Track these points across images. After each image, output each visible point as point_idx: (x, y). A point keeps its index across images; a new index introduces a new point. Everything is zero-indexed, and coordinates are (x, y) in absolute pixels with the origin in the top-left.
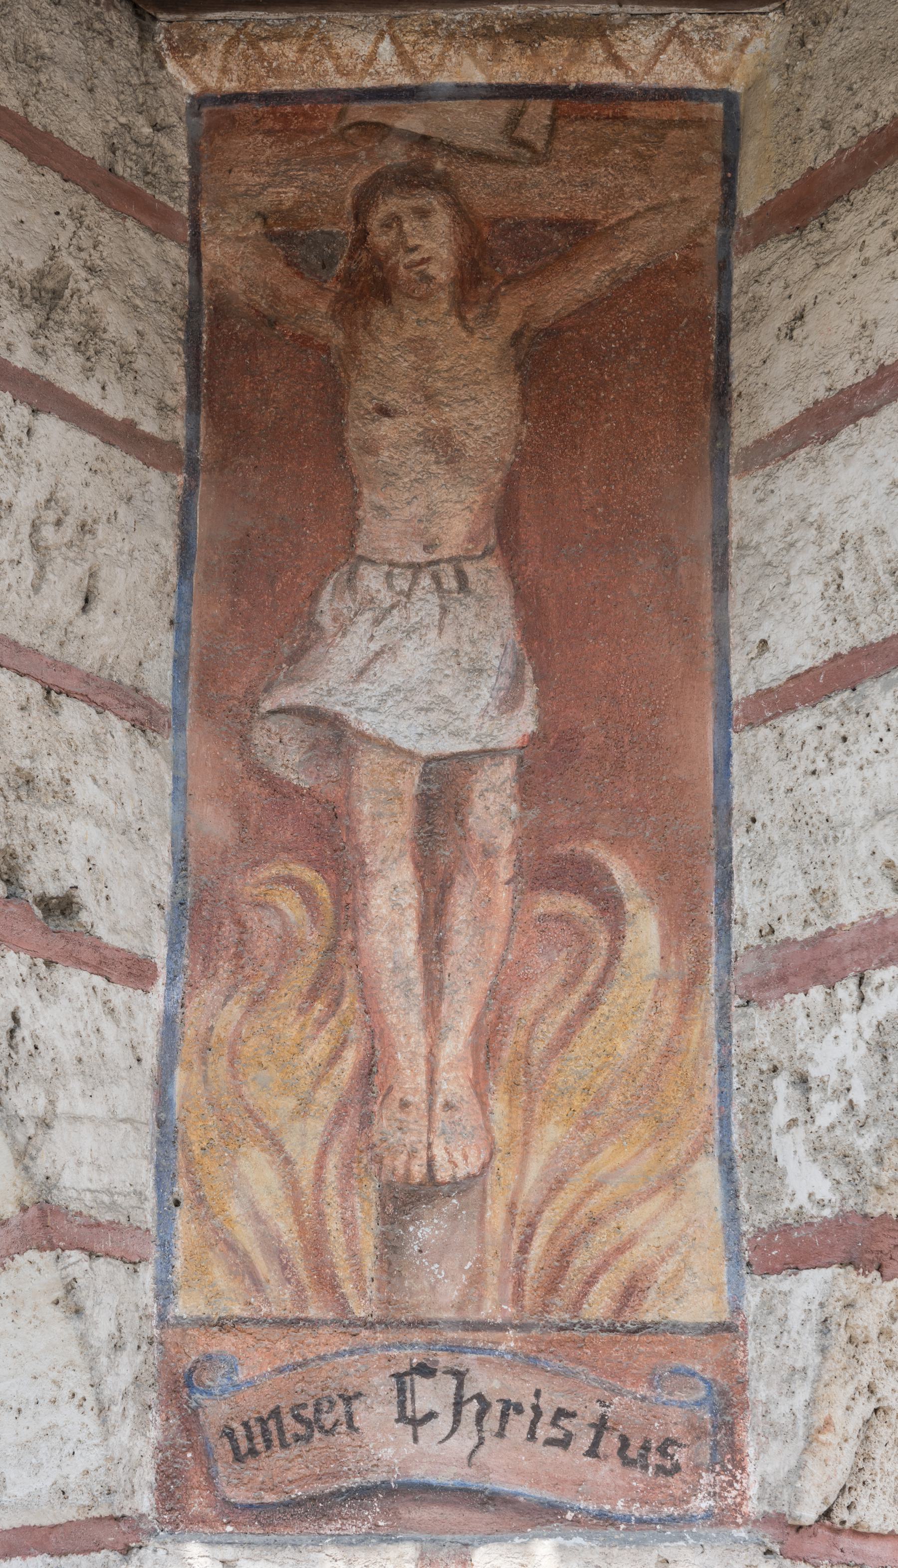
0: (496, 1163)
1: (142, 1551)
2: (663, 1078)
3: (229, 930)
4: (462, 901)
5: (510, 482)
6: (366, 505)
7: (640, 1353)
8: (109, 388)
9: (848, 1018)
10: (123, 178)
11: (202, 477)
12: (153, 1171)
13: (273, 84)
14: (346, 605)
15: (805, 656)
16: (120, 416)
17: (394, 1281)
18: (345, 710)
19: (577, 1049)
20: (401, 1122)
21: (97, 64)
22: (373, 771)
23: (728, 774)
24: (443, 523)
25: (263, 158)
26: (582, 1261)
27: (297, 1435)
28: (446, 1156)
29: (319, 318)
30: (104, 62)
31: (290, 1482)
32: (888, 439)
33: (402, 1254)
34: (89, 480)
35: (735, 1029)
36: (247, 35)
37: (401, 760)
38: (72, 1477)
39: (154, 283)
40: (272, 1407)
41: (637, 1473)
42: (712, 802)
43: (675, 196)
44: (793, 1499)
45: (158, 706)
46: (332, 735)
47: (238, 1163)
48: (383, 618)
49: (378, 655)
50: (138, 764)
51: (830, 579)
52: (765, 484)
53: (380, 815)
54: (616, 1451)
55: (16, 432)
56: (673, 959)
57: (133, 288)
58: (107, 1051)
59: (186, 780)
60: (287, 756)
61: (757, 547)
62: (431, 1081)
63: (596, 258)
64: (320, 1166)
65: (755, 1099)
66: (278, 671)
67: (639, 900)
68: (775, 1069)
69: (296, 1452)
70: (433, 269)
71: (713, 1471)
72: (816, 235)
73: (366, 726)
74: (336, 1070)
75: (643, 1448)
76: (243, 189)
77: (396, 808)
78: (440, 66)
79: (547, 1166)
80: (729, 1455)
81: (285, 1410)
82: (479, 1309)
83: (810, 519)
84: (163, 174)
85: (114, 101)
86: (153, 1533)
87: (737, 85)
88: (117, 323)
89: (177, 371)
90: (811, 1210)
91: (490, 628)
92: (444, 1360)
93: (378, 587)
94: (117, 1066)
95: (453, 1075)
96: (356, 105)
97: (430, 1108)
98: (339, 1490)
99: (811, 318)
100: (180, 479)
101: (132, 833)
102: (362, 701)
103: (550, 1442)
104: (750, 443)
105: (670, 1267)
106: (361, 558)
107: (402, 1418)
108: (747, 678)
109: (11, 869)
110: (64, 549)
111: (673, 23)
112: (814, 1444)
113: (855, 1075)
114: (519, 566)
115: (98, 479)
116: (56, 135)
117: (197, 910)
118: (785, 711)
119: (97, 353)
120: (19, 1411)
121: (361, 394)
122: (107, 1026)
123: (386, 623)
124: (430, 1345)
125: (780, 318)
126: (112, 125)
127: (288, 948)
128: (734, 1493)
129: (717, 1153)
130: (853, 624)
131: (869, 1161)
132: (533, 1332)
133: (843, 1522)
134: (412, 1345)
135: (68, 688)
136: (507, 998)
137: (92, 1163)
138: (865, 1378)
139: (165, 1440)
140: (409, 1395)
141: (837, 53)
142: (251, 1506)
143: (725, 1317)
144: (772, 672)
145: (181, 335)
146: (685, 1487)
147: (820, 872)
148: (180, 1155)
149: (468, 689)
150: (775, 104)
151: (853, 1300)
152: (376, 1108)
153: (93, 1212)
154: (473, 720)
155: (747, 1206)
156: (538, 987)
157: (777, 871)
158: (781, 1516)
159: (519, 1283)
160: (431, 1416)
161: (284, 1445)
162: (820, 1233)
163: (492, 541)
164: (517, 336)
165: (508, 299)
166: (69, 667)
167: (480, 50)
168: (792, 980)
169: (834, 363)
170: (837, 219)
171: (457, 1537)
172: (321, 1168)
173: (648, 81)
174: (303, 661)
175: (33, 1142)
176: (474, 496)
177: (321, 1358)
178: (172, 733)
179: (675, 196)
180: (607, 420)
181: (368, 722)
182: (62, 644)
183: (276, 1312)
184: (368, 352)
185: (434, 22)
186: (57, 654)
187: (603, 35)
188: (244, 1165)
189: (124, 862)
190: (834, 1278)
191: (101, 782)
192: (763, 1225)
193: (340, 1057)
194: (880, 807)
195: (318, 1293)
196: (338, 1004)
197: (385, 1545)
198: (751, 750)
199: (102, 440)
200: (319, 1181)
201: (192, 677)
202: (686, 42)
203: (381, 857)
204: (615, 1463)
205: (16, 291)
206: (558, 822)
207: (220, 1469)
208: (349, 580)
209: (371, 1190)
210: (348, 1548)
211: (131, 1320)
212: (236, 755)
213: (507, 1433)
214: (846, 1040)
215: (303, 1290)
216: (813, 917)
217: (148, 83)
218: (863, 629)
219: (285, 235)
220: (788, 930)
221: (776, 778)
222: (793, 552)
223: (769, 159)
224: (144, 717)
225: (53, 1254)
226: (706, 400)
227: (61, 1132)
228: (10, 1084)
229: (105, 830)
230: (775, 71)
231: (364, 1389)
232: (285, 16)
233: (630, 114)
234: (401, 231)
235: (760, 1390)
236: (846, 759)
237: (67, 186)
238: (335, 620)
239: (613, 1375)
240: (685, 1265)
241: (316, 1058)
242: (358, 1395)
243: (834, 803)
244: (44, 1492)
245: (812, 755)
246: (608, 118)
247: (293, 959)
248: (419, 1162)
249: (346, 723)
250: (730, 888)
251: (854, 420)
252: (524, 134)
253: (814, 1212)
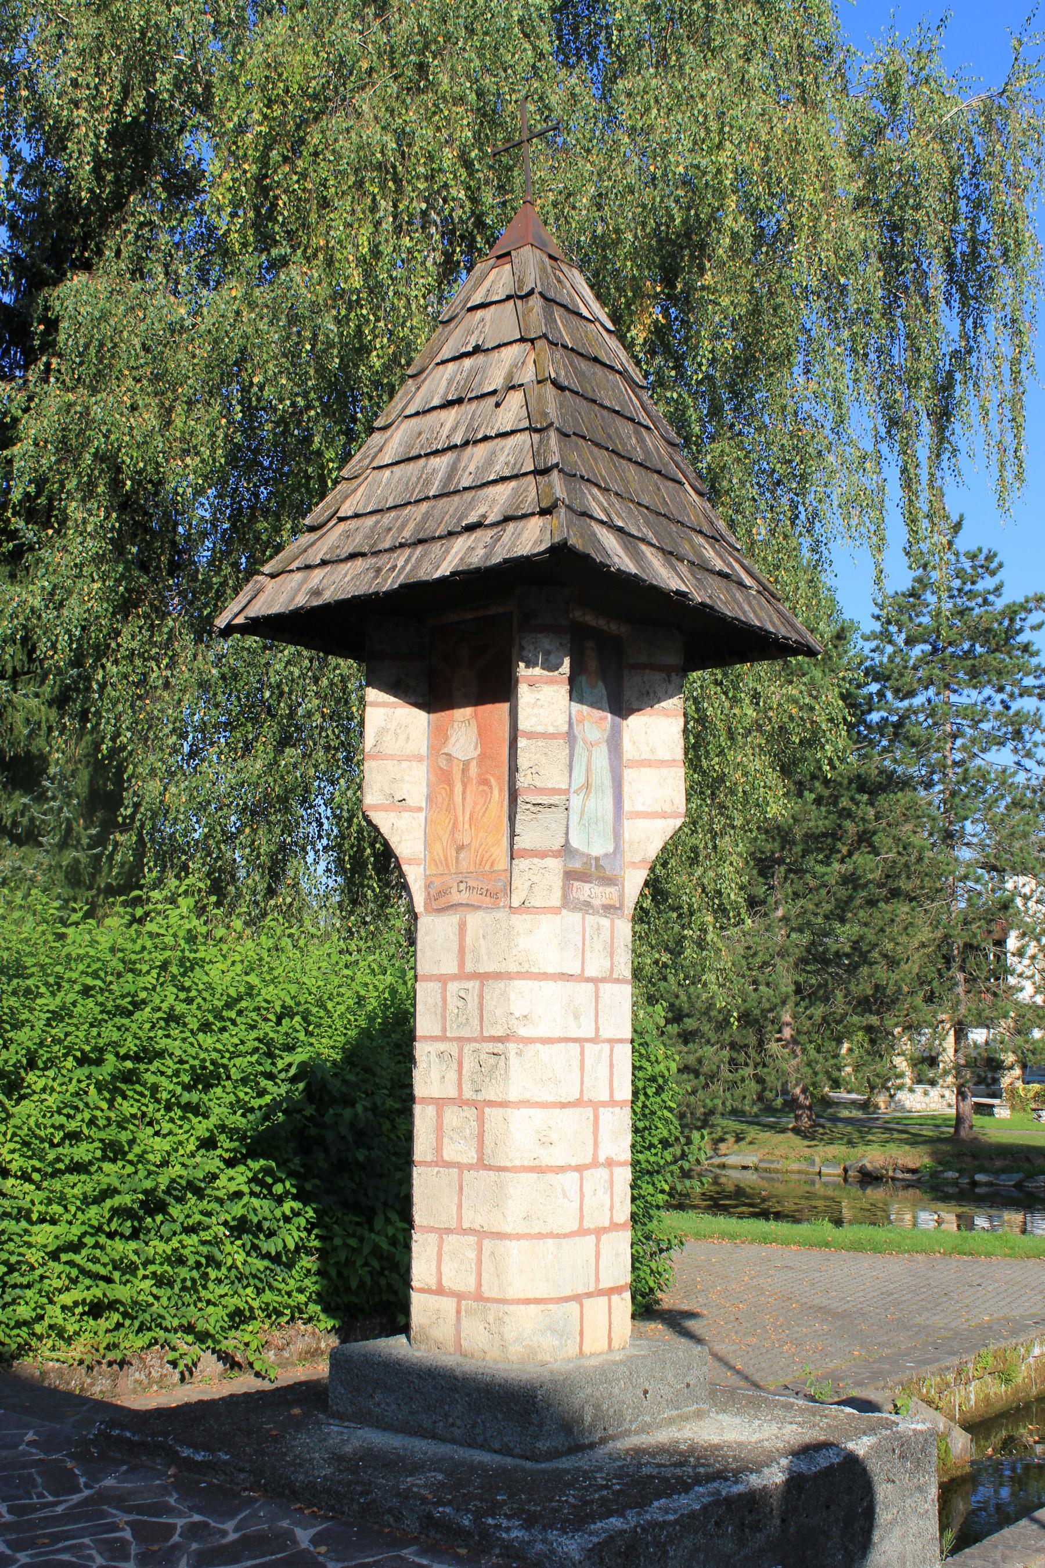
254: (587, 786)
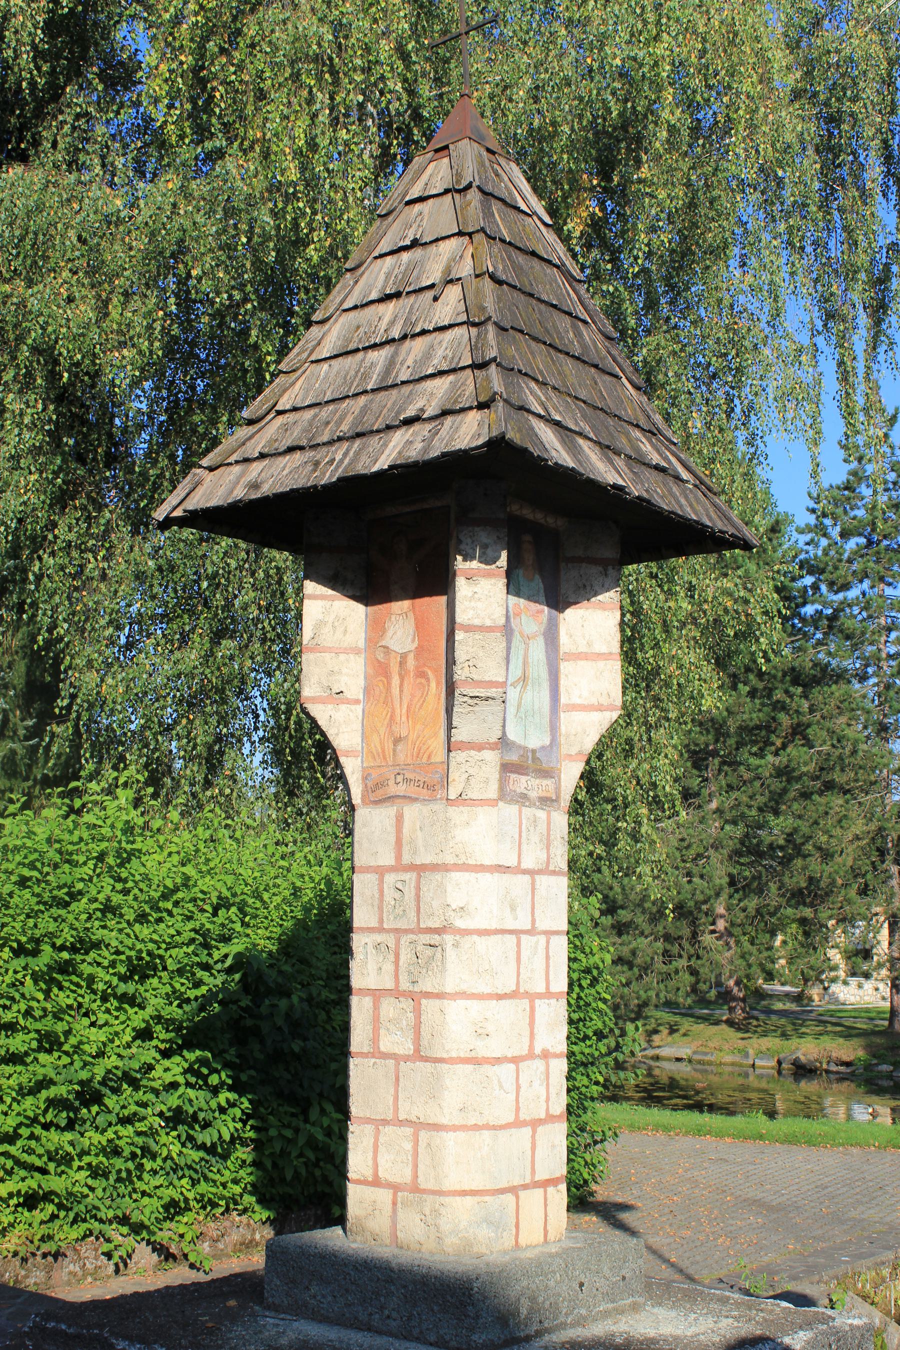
254: (524, 679)
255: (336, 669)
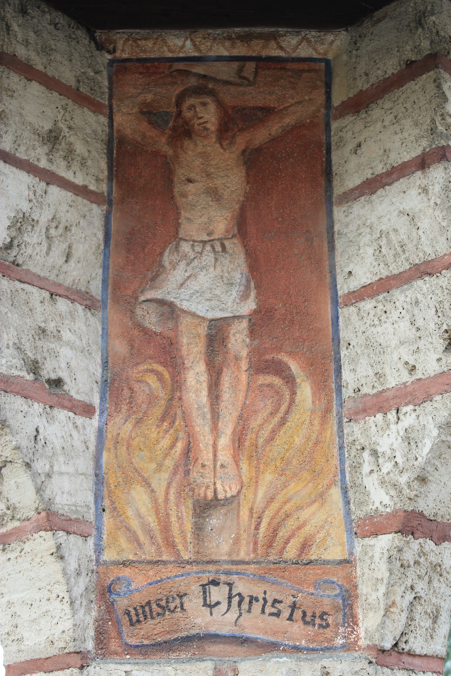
0: (244, 490)
1: (89, 668)
2: (315, 453)
3: (126, 393)
4: (226, 379)
5: (243, 209)
6: (182, 218)
7: (310, 574)
8: (77, 174)
9: (393, 427)
10: (82, 92)
11: (114, 206)
12: (93, 496)
13: (143, 55)
14: (175, 257)
15: (367, 278)
16: (81, 184)
17: (200, 543)
18: (175, 300)
19: (278, 441)
20: (202, 473)
21: (73, 51)
22: (187, 325)
23: (338, 325)
24: (215, 225)
25: (138, 83)
26: (283, 533)
27: (158, 613)
28: (222, 488)
29: (163, 144)
30: (76, 50)
31: (156, 634)
32: (397, 195)
33: (204, 531)
34: (69, 209)
35: (345, 432)
36: (132, 38)
37: (200, 320)
38: (57, 634)
39: (95, 132)
40: (147, 600)
41: (310, 628)
42: (331, 337)
43: (307, 98)
44: (380, 638)
45: (96, 299)
46: (170, 310)
47: (131, 492)
48: (191, 263)
49: (189, 277)
50: (88, 323)
51: (376, 248)
52: (348, 210)
53: (191, 344)
54: (300, 618)
55: (40, 193)
56: (317, 403)
57: (86, 134)
58: (74, 444)
59: (107, 329)
60: (151, 319)
61: (346, 234)
62: (215, 455)
63: (275, 121)
64: (167, 493)
65: (355, 461)
66: (147, 284)
67: (302, 378)
68: (363, 449)
69: (158, 621)
70: (209, 126)
71: (344, 626)
72: (364, 116)
73: (184, 307)
74: (173, 452)
75: (312, 616)
76: (130, 95)
77: (197, 340)
78: (210, 50)
79: (266, 492)
80: (351, 619)
81: (153, 602)
82: (238, 555)
83: (367, 224)
84: (98, 90)
85: (79, 64)
86: (93, 659)
87: (330, 56)
88: (80, 148)
89: (104, 165)
90: (381, 509)
91: (236, 266)
92: (223, 578)
93: (188, 250)
94: (79, 451)
95: (224, 453)
96: (176, 63)
97: (215, 467)
98: (177, 638)
99: (364, 147)
100: (105, 207)
101: (85, 352)
102: (182, 297)
103: (271, 614)
104: (341, 193)
105: (321, 535)
106: (181, 239)
107: (205, 605)
108: (343, 288)
109: (36, 368)
110: (58, 238)
111: (304, 35)
112: (388, 613)
113: (397, 451)
114: (247, 242)
115: (72, 209)
116: (57, 78)
117: (113, 383)
118: (360, 300)
119: (72, 160)
120: (32, 605)
121: (180, 174)
122: (75, 434)
123: (192, 265)
124: (217, 572)
125: (351, 146)
126: (79, 73)
127: (152, 399)
128: (354, 636)
129: (340, 485)
130: (387, 266)
131: (405, 487)
132: (262, 565)
133: (403, 649)
134: (209, 572)
135: (60, 293)
136: (247, 420)
137: (68, 493)
138: (409, 583)
139: (99, 616)
140: (208, 594)
141: (369, 48)
142: (138, 646)
143: (346, 557)
144: (354, 284)
145: (105, 151)
146: (332, 634)
147: (378, 366)
148: (105, 489)
149: (227, 292)
150: (346, 65)
151: (402, 548)
152: (191, 467)
153: (68, 514)
154: (229, 304)
155: (354, 508)
156: (260, 415)
157: (360, 366)
158: (375, 646)
159: (256, 543)
160: (218, 603)
161: (152, 618)
162: (386, 519)
163: (236, 232)
164: (244, 152)
165: (240, 137)
166: (60, 285)
167: (226, 44)
168: (368, 411)
169: (373, 164)
170: (372, 110)
171: (231, 658)
172: (167, 494)
173: (294, 55)
174: (157, 280)
175: (44, 484)
176: (228, 214)
177: (169, 578)
178: (101, 310)
179: (307, 98)
180: (282, 184)
181: (185, 305)
182: (57, 275)
183: (148, 558)
184: (182, 157)
185: (208, 34)
186: (55, 280)
187: (275, 39)
188: (133, 493)
189: (82, 364)
190: (393, 538)
191: (73, 331)
192: (361, 516)
193: (175, 445)
194: (402, 340)
195: (167, 549)
196: (174, 423)
197: (199, 663)
198: (347, 316)
199: (74, 194)
200: (167, 499)
201: (110, 287)
202: (309, 41)
203: (191, 361)
204: (301, 623)
205: (41, 138)
206: (267, 346)
207: (124, 629)
208: (176, 248)
209: (190, 504)
210: (182, 664)
211: (84, 561)
212: (129, 319)
213: (252, 611)
214: (393, 436)
215: (160, 548)
216: (376, 384)
217: (92, 56)
218: (391, 268)
219: (149, 113)
220: (365, 390)
221: (358, 327)
222: (361, 237)
223: (344, 85)
224: (90, 304)
225: (52, 533)
226: (322, 176)
227: (55, 479)
228: (35, 459)
229: (74, 351)
230: (345, 53)
231: (188, 592)
232: (148, 31)
233: (287, 67)
234: (195, 111)
235: (364, 589)
236: (386, 320)
237: (61, 97)
238: (170, 263)
239: (299, 584)
240: (328, 534)
241: (165, 446)
242: (185, 594)
243: (383, 338)
244: (42, 642)
245: (372, 318)
246: (278, 68)
247: (154, 404)
248: (210, 491)
249: (176, 306)
250: (341, 372)
251: (383, 187)
252: (245, 74)
253: (383, 510)
255: (51, 326)
